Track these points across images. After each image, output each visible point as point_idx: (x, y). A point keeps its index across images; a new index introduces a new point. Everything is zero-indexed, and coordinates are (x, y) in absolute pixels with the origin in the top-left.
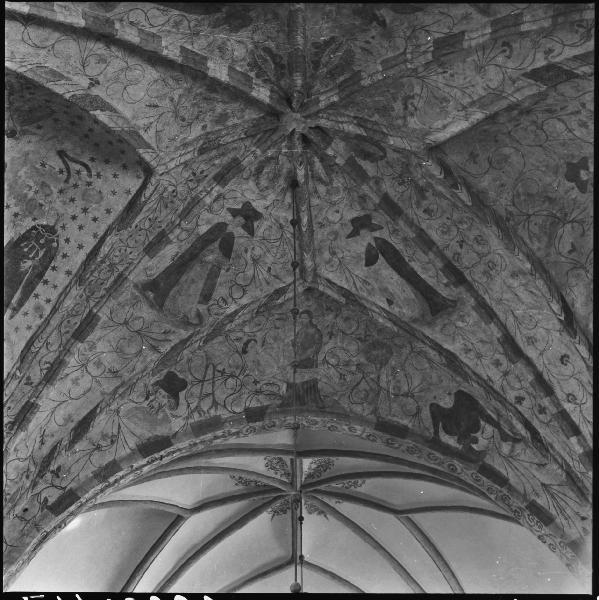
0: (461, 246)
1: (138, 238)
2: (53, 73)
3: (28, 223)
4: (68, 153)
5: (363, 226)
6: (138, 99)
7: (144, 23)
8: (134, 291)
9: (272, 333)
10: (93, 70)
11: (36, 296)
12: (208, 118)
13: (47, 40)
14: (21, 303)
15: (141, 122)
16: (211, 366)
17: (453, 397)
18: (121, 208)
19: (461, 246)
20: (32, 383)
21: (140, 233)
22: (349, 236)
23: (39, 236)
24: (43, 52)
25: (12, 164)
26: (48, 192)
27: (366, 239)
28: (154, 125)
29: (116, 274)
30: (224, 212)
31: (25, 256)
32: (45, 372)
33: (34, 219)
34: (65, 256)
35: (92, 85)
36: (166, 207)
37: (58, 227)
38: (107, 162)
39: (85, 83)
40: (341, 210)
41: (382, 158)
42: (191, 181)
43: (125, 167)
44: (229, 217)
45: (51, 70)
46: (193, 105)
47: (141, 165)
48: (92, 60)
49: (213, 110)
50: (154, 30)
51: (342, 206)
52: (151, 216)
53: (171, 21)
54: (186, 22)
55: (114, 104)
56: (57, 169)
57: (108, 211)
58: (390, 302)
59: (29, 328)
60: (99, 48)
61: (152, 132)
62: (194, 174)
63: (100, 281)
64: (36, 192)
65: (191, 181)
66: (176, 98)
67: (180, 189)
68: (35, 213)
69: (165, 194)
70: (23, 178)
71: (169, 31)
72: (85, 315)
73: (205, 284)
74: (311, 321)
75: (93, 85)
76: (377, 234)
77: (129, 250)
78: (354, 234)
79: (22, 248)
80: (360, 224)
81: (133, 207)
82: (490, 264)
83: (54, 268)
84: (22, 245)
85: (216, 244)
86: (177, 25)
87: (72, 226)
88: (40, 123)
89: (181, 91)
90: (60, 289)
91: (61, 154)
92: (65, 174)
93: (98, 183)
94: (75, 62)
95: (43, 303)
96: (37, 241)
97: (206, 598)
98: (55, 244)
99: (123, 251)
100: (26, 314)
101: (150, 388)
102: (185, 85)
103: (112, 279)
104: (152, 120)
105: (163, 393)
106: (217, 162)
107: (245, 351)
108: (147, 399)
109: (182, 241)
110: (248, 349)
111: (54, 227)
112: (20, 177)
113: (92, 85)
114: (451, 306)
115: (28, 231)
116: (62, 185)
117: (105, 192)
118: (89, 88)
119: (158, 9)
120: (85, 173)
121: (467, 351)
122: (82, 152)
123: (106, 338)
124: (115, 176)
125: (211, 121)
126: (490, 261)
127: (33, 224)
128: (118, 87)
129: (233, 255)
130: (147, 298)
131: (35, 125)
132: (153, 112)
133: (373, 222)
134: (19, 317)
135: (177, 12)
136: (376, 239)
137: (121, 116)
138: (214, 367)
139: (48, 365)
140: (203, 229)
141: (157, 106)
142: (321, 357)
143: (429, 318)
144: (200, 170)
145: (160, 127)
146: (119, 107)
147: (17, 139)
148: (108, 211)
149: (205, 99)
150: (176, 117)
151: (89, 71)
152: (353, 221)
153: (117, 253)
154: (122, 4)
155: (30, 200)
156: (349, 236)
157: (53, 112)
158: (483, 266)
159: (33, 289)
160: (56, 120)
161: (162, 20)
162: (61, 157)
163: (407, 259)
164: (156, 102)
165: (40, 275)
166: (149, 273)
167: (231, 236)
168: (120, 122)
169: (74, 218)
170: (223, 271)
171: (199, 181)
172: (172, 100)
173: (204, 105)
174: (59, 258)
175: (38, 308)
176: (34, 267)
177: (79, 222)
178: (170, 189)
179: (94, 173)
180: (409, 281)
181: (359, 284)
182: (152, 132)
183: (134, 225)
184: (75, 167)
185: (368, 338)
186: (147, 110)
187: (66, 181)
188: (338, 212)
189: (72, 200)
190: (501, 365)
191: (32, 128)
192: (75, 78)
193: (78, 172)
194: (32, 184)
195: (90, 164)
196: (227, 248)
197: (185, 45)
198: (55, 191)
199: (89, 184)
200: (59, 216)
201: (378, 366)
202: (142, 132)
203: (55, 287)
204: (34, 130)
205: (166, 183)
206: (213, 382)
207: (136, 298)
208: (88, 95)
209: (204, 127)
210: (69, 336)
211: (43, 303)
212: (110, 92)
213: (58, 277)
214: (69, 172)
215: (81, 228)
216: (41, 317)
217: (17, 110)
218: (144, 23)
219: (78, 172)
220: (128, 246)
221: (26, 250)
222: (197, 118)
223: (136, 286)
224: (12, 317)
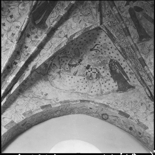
1: (121, 37)
2: (59, 46)
3: (107, 65)
4: (92, 48)
6: (76, 25)
7: (54, 18)
8: (139, 44)
10: (62, 35)
11: (127, 72)
12: (92, 6)
13: (49, 45)
14: (127, 77)
15: (84, 26)
18: (110, 39)
20: (151, 86)
21: (120, 36)
23: (112, 64)
24: (52, 46)
25: (89, 63)
26: (101, 57)
29: (131, 48)
30: (125, 8)
31: (116, 70)
32: (149, 80)
33: (107, 63)
34: (119, 60)
36: (115, 26)
37: (112, 58)
38: (96, 39)
39: (65, 38)
42: (110, 16)
43: (98, 34)
44: (128, 6)
45: (58, 46)
46: (86, 9)
47: (98, 30)
48: (60, 35)
49: (89, 4)
50: (57, 16)
52: (116, 31)
53: (56, 11)
54: (58, 7)
55: (75, 32)
56: (96, 52)
57: (110, 43)
59: (135, 78)
60: (57, 32)
61: (88, 24)
62: (108, 14)
63: (130, 53)
64: (100, 60)
65: (110, 16)
66: (81, 14)
67: (111, 20)
68: (105, 63)
69: (110, 25)
70: (95, 62)
71: (59, 12)
72: (139, 61)
73: (149, 20)
75: (67, 36)
77: (124, 41)
79: (113, 70)
81: (110, 35)
83: (121, 64)
84: (112, 69)
85: (137, 13)
86: (58, 9)
87: (112, 55)
88: (126, 72)
89: (79, 13)
90: (128, 65)
91: (91, 50)
92: (97, 51)
93: (102, 43)
94: (58, 39)
95: (130, 71)
96: (113, 65)
97: (55, 154)
98: (115, 61)
99: (124, 43)
100: (131, 77)
102: (78, 11)
103: (132, 49)
104: (84, 23)
106: (107, 6)
109: (129, 24)
111: (111, 59)
112: (94, 62)
113: (67, 37)
115: (109, 67)
116: (100, 53)
117: (104, 42)
118: (67, 38)
119: (52, 14)
120: (98, 46)
122: (92, 44)
123: (151, 58)
124: (100, 38)
125: (93, 5)
127: (108, 64)
128: (70, 30)
129: (142, 8)
130: (145, 41)
131: (81, 54)
132: (82, 22)
134: (131, 80)
135: (54, 9)
137: (78, 32)
139: (148, 79)
140: (129, 16)
141: (81, 20)
144: (108, 12)
145: (88, 21)
146: (77, 31)
147: (83, 59)
148: (110, 43)
149: (85, 5)
150: (87, 16)
151: (62, 36)
153: (124, 45)
154: (153, 26)
155: (101, 62)
157: (77, 48)
159: (125, 72)
160: (80, 48)
161: (55, 13)
162: (92, 50)
164: (79, 20)
165: (122, 68)
166: (136, 37)
167: (135, 7)
168: (80, 32)
170: (147, 13)
171: (111, 13)
172: (81, 16)
173: (87, 6)
174: (119, 62)
175: (131, 73)
176: (119, 69)
177: (111, 52)
178: (109, 23)
179: (98, 43)
182: (88, 24)
183: (116, 37)
184: (96, 48)
186: (80, 24)
187: (100, 51)
189: (105, 52)
191: (81, 55)
192: (63, 40)
193: (98, 47)
194: (97, 60)
195: (96, 44)
197: (65, 8)
198: (101, 55)
199: (101, 46)
200: (108, 57)
202: (87, 27)
203: (127, 66)
204: (82, 55)
205: (107, 24)
207: (142, 44)
208: (68, 39)
209: (94, 8)
210: (143, 69)
211: (130, 71)
212: (71, 33)
213: (124, 64)
214: (97, 50)
215: (113, 52)
216: (133, 74)
217: (73, 57)
218: (54, 18)
219: (98, 47)
220: (123, 41)
221: (114, 69)
222: (90, 9)
223: (138, 43)
224: (130, 81)
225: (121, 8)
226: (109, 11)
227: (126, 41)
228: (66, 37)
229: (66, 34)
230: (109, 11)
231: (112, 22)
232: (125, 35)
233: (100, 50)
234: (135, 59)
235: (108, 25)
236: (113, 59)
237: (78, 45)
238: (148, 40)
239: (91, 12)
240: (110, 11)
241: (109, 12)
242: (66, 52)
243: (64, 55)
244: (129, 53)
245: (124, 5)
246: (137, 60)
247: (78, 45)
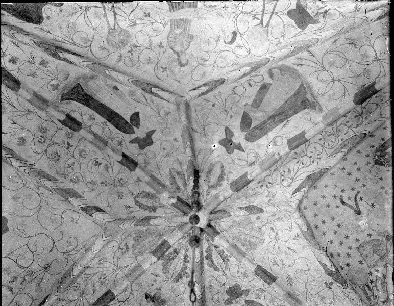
0: (69, 144)
5: (145, 140)
9: (211, 47)
16: (265, 24)
17: (44, 16)
19: (69, 144)
22: (153, 131)
27: (140, 133)
28: (292, 237)
29: (335, 126)
35: (331, 284)
36: (289, 170)
40: (162, 150)
41: (137, 196)
42: (270, 183)
51: (162, 153)
58: (116, 88)
62: (267, 186)
63: (349, 124)
65: (270, 183)
69: (290, 181)
74: (178, 56)
76: (133, 136)
78: (150, 134)
80: (146, 142)
82: (43, 140)
88: (368, 238)
98: (378, 154)
101: (321, 20)
103: (339, 123)
105: (310, 12)
107: (235, 34)
108: (326, 11)
110: (231, 36)
111: (376, 164)
113: (331, 284)
114: (66, 94)
121: (43, 63)
126: (44, 142)
130: (312, 94)
131: (372, 238)
133: (137, 145)
136: (134, 132)
138: (262, 23)
142: (168, 27)
143: (82, 82)
152: (151, 143)
156: (153, 131)
158: (48, 136)
162: (360, 210)
163: (108, 123)
169: (359, 170)
178: (285, 183)
179: (338, 198)
180: (103, 106)
181: (142, 99)
185: (130, 49)
188: (164, 149)
190: (10, 61)
193: (349, 198)
196: (246, 121)
201: (116, 27)
206: (263, 12)
214: (356, 200)
225: (249, 159)
226: (260, 184)
227: (320, 139)
228: (331, 285)
229: (324, 286)
230: (260, 184)
231: (282, 178)
232: (306, 143)
233: (355, 193)
234: (362, 113)
235: (289, 185)
236: (374, 158)
237: (350, 248)
238: (310, 87)
239: (267, 225)
240: (259, 182)
241: (262, 185)
242: (372, 282)
243: (380, 287)
244: (349, 127)
245: (243, 153)
246: (364, 107)
247: (350, 248)
